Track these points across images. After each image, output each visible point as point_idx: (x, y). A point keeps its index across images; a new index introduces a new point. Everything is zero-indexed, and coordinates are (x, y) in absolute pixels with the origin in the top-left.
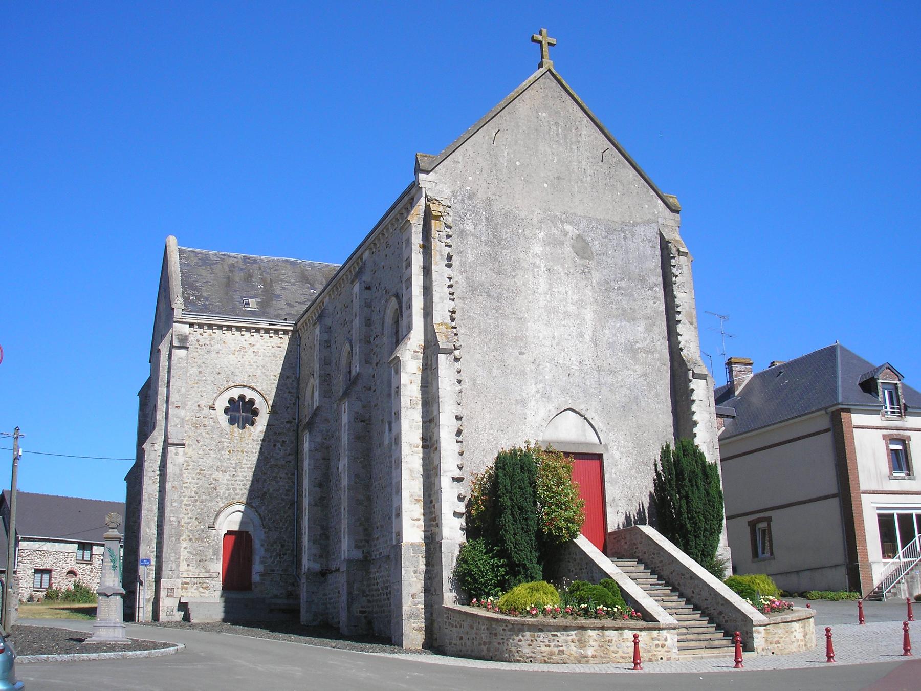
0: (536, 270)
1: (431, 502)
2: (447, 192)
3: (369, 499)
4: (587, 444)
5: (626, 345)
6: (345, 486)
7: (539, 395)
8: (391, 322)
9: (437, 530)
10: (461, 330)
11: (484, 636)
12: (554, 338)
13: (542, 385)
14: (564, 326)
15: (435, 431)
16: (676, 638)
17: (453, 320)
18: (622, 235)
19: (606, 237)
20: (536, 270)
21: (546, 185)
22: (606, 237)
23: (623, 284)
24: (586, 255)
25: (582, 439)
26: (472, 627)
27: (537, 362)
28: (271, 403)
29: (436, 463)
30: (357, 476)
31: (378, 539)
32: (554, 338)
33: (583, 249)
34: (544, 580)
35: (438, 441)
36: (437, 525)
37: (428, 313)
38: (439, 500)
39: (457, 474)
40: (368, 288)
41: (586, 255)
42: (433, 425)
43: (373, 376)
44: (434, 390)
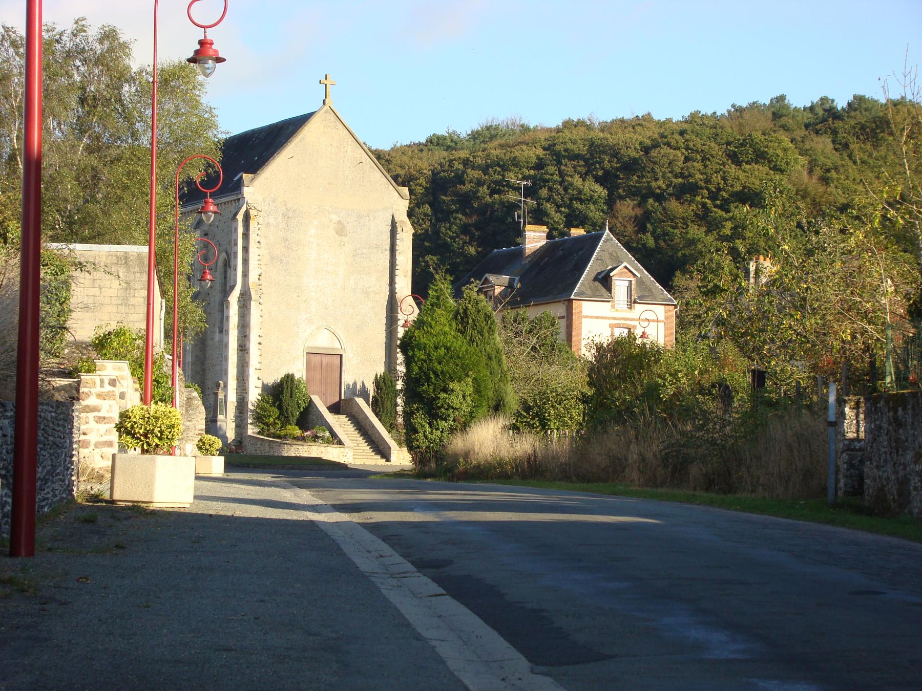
0: (310, 245)
1: (244, 380)
2: (260, 199)
3: (204, 370)
4: (333, 349)
5: (362, 289)
6: (189, 362)
7: (307, 321)
8: (222, 264)
9: (246, 395)
10: (264, 284)
11: (267, 449)
12: (318, 287)
13: (309, 315)
14: (325, 279)
15: (247, 342)
16: (353, 453)
17: (259, 279)
18: (368, 218)
19: (357, 221)
20: (310, 245)
21: (321, 189)
22: (357, 221)
23: (365, 251)
24: (343, 234)
25: (331, 346)
26: (262, 445)
27: (307, 301)
28: (444, 592)
29: (247, 360)
30: (197, 356)
31: (209, 395)
32: (318, 287)
33: (341, 230)
34: (296, 425)
35: (248, 349)
36: (246, 393)
37: (245, 275)
38: (248, 380)
39: (258, 366)
40: (206, 235)
41: (343, 234)
42: (246, 339)
43: (209, 294)
44: (248, 320)
